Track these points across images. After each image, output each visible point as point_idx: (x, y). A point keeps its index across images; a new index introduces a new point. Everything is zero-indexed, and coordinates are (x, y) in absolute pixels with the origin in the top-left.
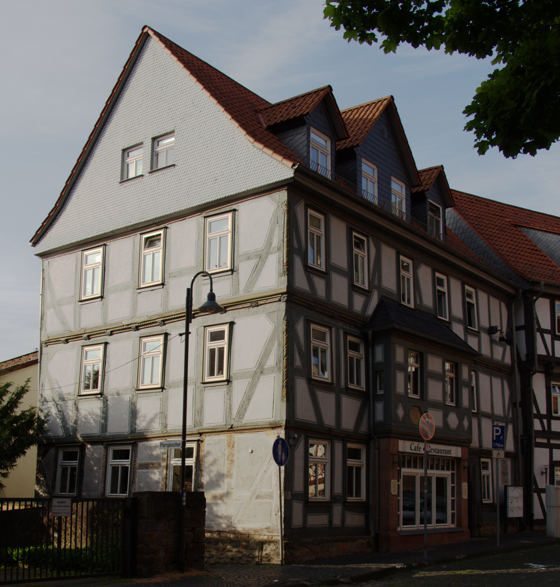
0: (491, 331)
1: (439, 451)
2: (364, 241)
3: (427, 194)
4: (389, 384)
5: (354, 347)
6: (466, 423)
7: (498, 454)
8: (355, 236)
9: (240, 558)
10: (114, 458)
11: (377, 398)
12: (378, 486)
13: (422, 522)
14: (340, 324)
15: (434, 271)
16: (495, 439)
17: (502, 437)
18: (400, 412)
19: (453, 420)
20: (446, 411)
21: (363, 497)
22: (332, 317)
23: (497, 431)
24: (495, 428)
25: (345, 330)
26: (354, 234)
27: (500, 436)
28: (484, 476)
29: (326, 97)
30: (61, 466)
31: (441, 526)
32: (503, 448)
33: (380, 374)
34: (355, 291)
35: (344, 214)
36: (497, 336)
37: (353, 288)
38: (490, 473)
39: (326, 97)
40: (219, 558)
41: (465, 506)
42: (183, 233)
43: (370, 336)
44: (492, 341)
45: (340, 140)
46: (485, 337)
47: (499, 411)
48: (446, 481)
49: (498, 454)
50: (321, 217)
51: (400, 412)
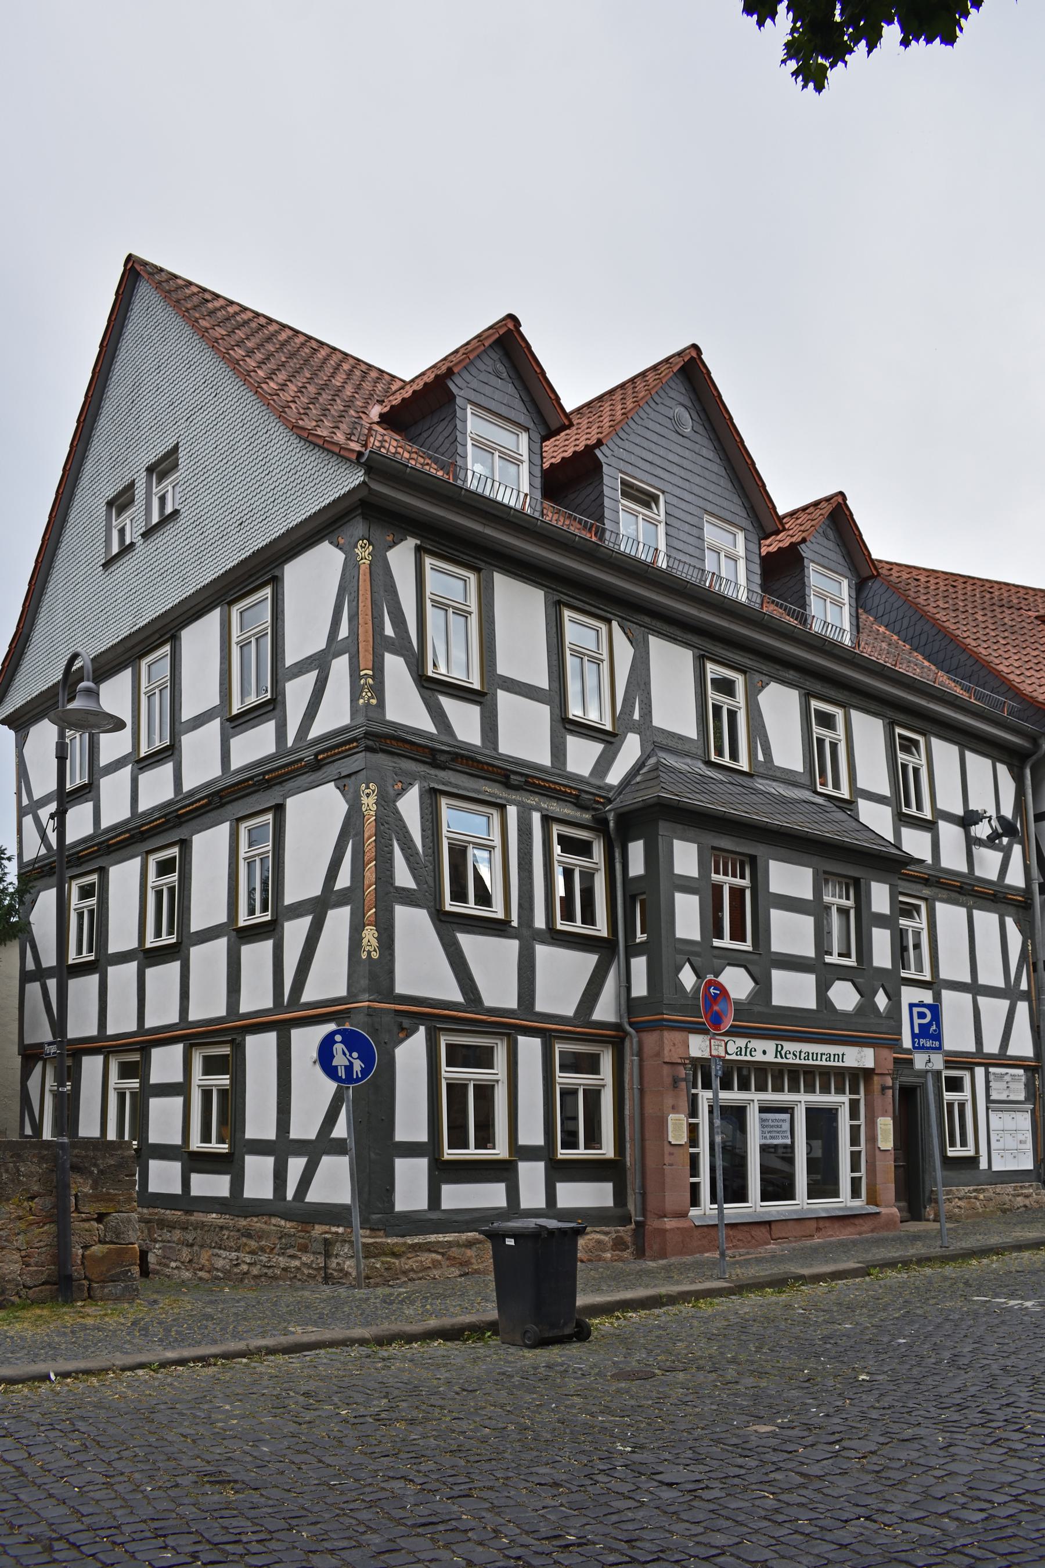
0: (968, 820)
1: (815, 1056)
2: (918, 741)
3: (805, 551)
4: (659, 919)
5: (582, 848)
6: (881, 1000)
7: (929, 1061)
8: (899, 735)
9: (298, 1269)
10: (205, 1073)
11: (633, 950)
12: (638, 1126)
13: (813, 1192)
14: (532, 800)
15: (807, 696)
16: (917, 1031)
17: (934, 1027)
18: (687, 978)
19: (844, 997)
20: (826, 976)
21: (607, 1150)
22: (508, 785)
23: (921, 1015)
24: (915, 1010)
25: (545, 813)
26: (898, 730)
27: (930, 1024)
28: (950, 1105)
29: (506, 345)
30: (199, 1086)
31: (824, 1205)
32: (940, 1048)
33: (643, 901)
34: (572, 732)
35: (679, 629)
36: (982, 830)
37: (565, 725)
38: (969, 1097)
39: (506, 345)
40: (265, 1266)
41: (887, 1167)
42: (201, 639)
43: (612, 824)
44: (971, 842)
45: (766, 538)
46: (950, 834)
47: (991, 975)
48: (836, 1114)
49: (929, 1061)
50: (921, 739)
51: (687, 978)
